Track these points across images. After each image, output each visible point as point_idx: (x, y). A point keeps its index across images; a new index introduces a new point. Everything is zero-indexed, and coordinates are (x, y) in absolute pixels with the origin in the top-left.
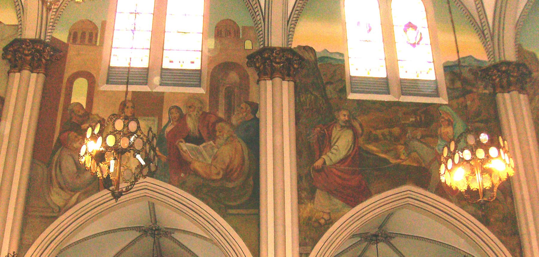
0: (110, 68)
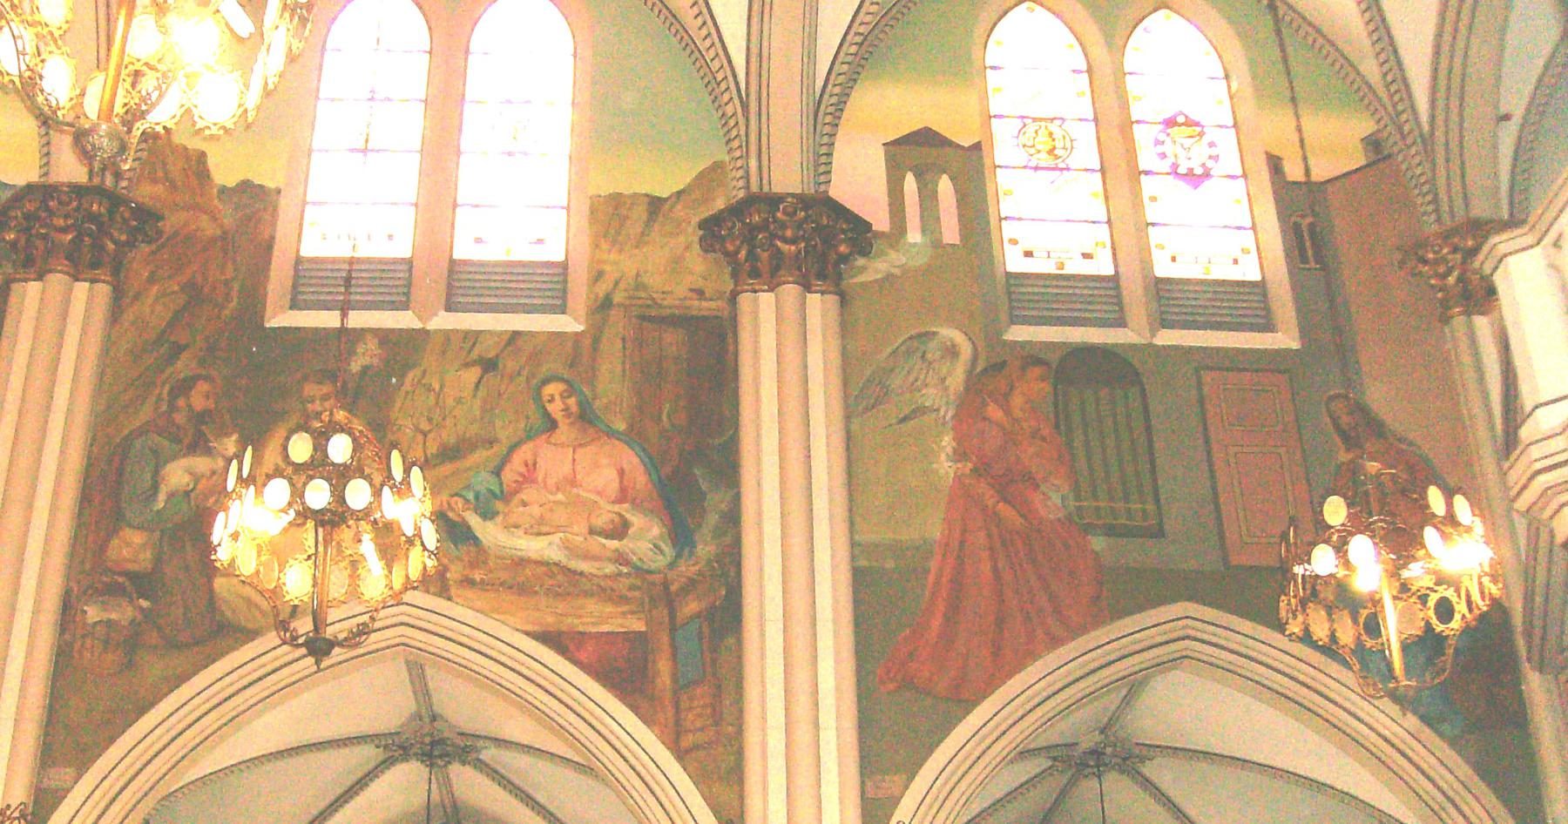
0: (299, 260)
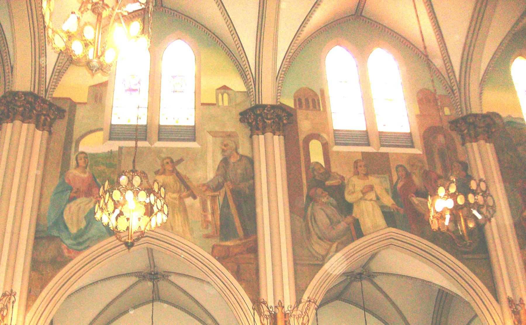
0: (111, 125)
